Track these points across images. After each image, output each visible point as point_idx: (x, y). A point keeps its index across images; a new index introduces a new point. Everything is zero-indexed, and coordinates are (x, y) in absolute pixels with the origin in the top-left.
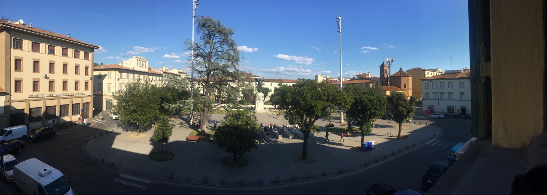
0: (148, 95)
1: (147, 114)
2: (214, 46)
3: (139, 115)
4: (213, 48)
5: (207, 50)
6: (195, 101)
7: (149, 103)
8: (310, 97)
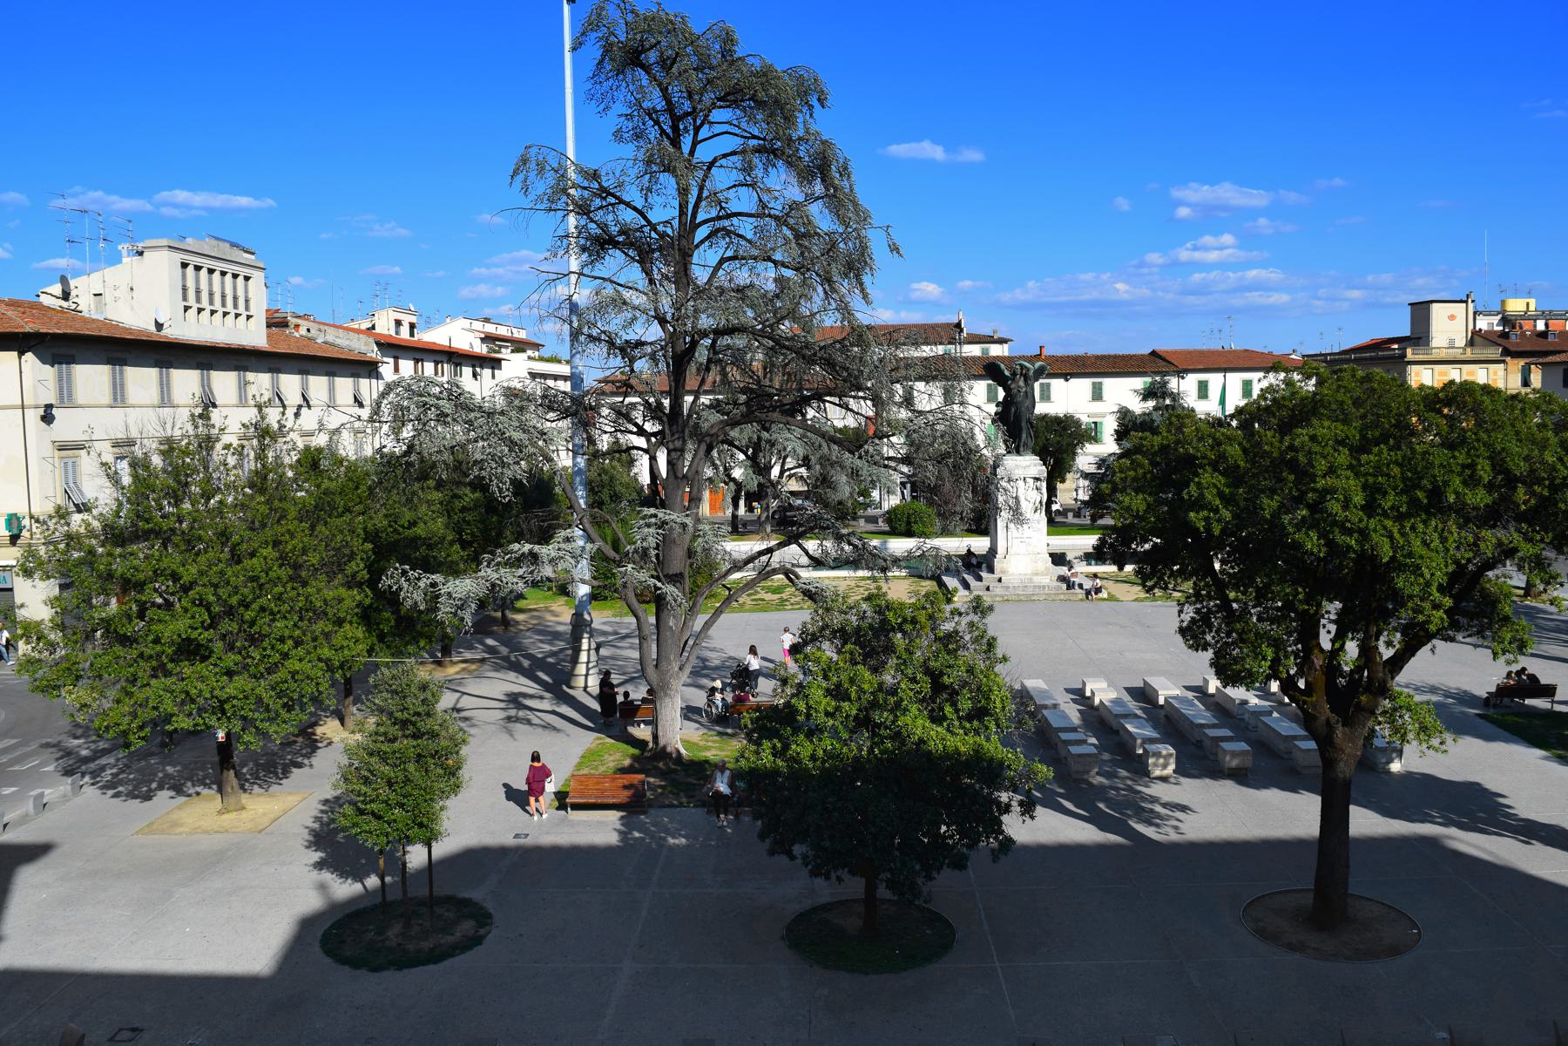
0: (279, 529)
1: (285, 656)
2: (701, 189)
3: (230, 674)
4: (699, 199)
6: (599, 543)
7: (291, 579)
8: (1359, 499)
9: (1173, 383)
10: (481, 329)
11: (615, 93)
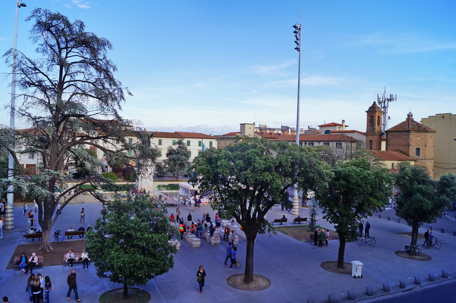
11: (39, 38)
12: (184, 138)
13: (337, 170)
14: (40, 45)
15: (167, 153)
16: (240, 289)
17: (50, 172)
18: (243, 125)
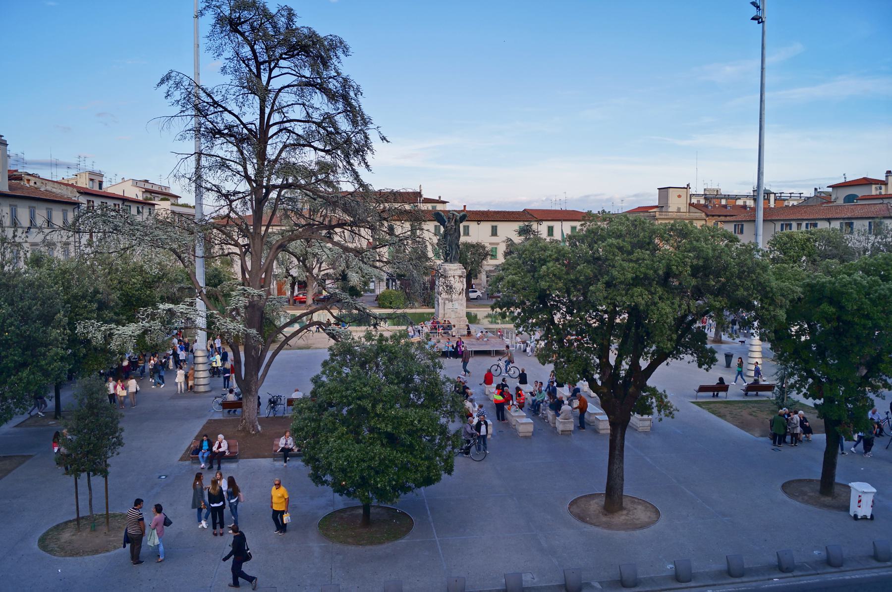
5: (251, 116)
9: (535, 226)
10: (143, 187)
11: (224, 47)
12: (542, 220)
13: (815, 282)
14: (228, 61)
15: (505, 252)
16: (591, 524)
17: (246, 291)
18: (664, 191)
